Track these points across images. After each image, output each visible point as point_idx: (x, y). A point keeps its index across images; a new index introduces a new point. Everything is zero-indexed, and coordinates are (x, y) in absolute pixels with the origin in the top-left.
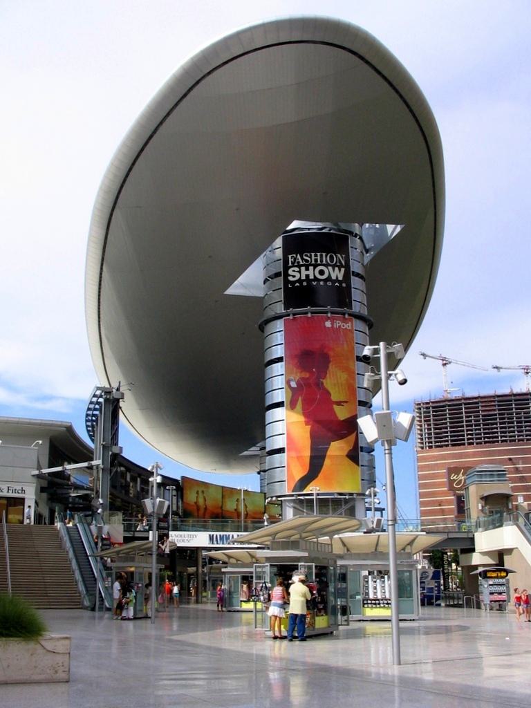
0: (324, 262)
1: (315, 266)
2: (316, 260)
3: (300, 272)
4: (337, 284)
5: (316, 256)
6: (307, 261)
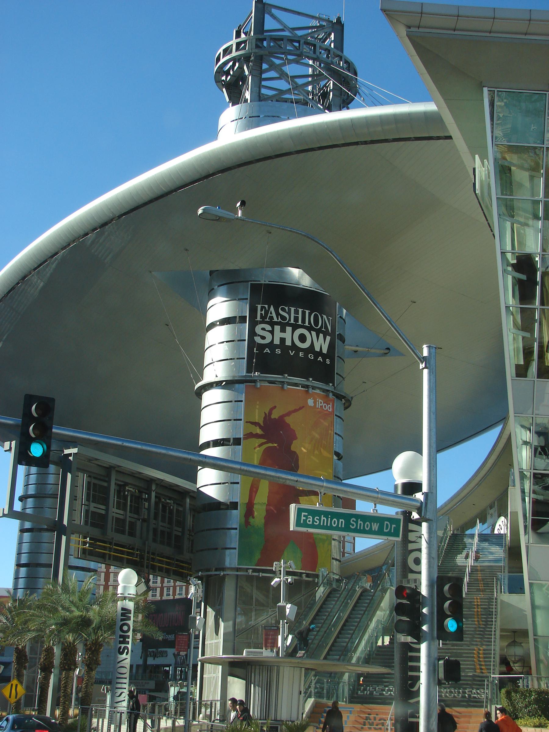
0: (307, 324)
1: (295, 327)
2: (296, 319)
3: (272, 332)
4: (320, 359)
5: (296, 312)
6: (283, 318)
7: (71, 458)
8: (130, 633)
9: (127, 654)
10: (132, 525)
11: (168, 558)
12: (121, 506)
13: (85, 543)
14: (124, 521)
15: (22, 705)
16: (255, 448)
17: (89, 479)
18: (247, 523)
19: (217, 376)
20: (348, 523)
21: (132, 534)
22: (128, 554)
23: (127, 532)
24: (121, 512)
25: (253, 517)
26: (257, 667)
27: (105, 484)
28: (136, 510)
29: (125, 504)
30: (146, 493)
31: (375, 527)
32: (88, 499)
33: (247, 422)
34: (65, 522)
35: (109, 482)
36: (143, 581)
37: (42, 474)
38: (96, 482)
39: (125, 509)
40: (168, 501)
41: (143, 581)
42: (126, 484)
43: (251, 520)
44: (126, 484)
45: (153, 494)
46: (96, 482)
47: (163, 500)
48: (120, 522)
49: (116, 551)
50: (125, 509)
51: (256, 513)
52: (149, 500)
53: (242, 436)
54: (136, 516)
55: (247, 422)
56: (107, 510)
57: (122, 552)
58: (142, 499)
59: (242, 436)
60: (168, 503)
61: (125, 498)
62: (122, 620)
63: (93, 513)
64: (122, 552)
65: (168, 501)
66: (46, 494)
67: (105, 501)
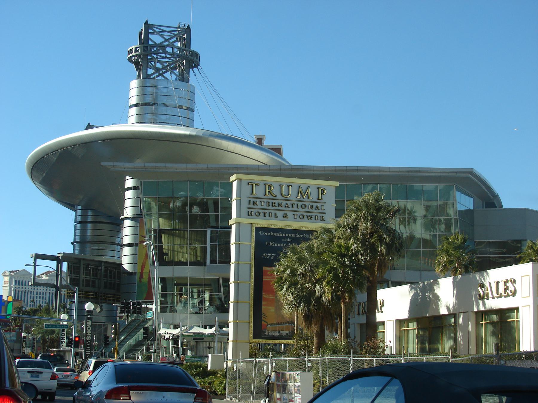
7: (60, 258)
8: (35, 344)
9: (64, 343)
10: (94, 282)
11: (113, 295)
12: (88, 274)
13: (70, 293)
14: (89, 281)
15: (376, 360)
16: (144, 248)
17: (71, 264)
18: (140, 281)
19: (127, 215)
20: (56, 327)
21: (93, 286)
22: (92, 295)
23: (91, 286)
24: (88, 277)
25: (143, 279)
26: (68, 352)
27: (79, 265)
28: (95, 275)
29: (90, 273)
30: (100, 267)
31: (62, 327)
32: (71, 273)
33: (140, 236)
34: (59, 286)
35: (80, 264)
36: (99, 306)
37: (186, 118)
38: (74, 265)
39: (90, 275)
40: (112, 269)
41: (99, 306)
42: (89, 265)
43: (142, 280)
44: (89, 265)
45: (103, 267)
46: (74, 265)
47: (109, 269)
48: (88, 281)
49: (85, 294)
50: (90, 275)
51: (144, 277)
52: (101, 270)
53: (138, 242)
54: (95, 278)
55: (140, 236)
56: (79, 277)
57: (89, 295)
58: (98, 270)
59: (138, 242)
60: (112, 270)
61: (90, 270)
62: (62, 332)
63: (74, 279)
64: (89, 295)
65: (112, 269)
66: (85, 241)
67: (79, 273)
